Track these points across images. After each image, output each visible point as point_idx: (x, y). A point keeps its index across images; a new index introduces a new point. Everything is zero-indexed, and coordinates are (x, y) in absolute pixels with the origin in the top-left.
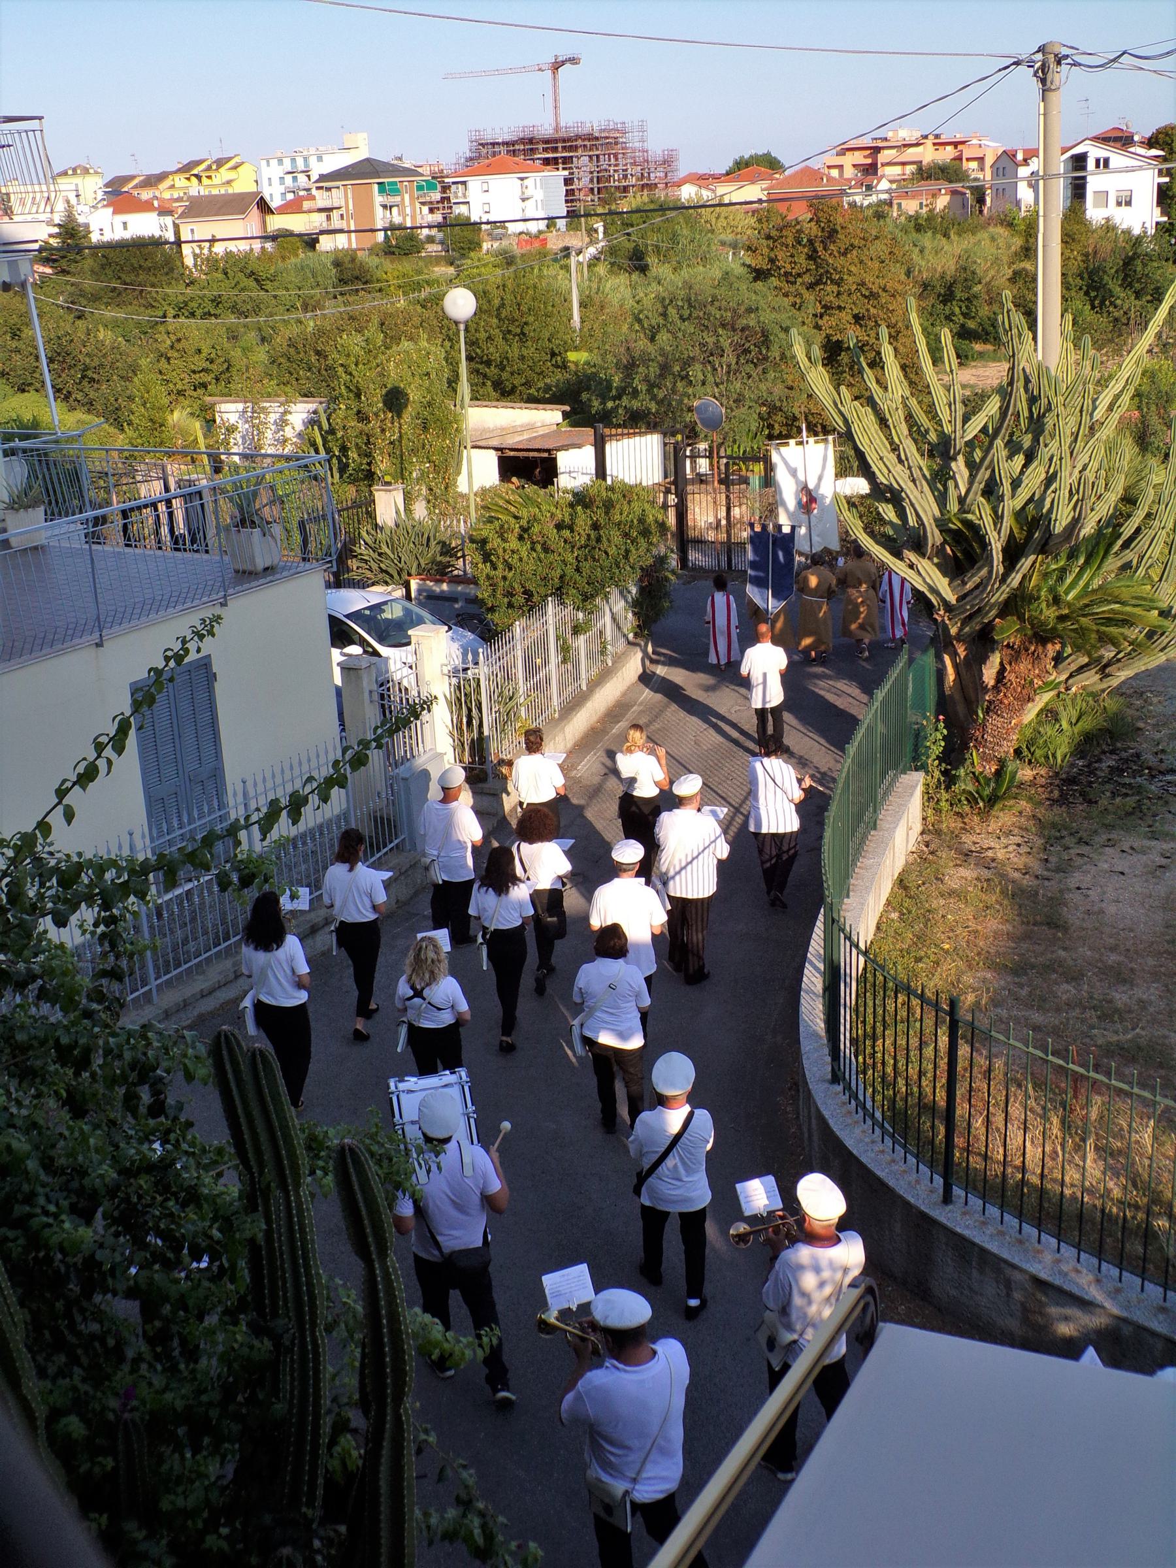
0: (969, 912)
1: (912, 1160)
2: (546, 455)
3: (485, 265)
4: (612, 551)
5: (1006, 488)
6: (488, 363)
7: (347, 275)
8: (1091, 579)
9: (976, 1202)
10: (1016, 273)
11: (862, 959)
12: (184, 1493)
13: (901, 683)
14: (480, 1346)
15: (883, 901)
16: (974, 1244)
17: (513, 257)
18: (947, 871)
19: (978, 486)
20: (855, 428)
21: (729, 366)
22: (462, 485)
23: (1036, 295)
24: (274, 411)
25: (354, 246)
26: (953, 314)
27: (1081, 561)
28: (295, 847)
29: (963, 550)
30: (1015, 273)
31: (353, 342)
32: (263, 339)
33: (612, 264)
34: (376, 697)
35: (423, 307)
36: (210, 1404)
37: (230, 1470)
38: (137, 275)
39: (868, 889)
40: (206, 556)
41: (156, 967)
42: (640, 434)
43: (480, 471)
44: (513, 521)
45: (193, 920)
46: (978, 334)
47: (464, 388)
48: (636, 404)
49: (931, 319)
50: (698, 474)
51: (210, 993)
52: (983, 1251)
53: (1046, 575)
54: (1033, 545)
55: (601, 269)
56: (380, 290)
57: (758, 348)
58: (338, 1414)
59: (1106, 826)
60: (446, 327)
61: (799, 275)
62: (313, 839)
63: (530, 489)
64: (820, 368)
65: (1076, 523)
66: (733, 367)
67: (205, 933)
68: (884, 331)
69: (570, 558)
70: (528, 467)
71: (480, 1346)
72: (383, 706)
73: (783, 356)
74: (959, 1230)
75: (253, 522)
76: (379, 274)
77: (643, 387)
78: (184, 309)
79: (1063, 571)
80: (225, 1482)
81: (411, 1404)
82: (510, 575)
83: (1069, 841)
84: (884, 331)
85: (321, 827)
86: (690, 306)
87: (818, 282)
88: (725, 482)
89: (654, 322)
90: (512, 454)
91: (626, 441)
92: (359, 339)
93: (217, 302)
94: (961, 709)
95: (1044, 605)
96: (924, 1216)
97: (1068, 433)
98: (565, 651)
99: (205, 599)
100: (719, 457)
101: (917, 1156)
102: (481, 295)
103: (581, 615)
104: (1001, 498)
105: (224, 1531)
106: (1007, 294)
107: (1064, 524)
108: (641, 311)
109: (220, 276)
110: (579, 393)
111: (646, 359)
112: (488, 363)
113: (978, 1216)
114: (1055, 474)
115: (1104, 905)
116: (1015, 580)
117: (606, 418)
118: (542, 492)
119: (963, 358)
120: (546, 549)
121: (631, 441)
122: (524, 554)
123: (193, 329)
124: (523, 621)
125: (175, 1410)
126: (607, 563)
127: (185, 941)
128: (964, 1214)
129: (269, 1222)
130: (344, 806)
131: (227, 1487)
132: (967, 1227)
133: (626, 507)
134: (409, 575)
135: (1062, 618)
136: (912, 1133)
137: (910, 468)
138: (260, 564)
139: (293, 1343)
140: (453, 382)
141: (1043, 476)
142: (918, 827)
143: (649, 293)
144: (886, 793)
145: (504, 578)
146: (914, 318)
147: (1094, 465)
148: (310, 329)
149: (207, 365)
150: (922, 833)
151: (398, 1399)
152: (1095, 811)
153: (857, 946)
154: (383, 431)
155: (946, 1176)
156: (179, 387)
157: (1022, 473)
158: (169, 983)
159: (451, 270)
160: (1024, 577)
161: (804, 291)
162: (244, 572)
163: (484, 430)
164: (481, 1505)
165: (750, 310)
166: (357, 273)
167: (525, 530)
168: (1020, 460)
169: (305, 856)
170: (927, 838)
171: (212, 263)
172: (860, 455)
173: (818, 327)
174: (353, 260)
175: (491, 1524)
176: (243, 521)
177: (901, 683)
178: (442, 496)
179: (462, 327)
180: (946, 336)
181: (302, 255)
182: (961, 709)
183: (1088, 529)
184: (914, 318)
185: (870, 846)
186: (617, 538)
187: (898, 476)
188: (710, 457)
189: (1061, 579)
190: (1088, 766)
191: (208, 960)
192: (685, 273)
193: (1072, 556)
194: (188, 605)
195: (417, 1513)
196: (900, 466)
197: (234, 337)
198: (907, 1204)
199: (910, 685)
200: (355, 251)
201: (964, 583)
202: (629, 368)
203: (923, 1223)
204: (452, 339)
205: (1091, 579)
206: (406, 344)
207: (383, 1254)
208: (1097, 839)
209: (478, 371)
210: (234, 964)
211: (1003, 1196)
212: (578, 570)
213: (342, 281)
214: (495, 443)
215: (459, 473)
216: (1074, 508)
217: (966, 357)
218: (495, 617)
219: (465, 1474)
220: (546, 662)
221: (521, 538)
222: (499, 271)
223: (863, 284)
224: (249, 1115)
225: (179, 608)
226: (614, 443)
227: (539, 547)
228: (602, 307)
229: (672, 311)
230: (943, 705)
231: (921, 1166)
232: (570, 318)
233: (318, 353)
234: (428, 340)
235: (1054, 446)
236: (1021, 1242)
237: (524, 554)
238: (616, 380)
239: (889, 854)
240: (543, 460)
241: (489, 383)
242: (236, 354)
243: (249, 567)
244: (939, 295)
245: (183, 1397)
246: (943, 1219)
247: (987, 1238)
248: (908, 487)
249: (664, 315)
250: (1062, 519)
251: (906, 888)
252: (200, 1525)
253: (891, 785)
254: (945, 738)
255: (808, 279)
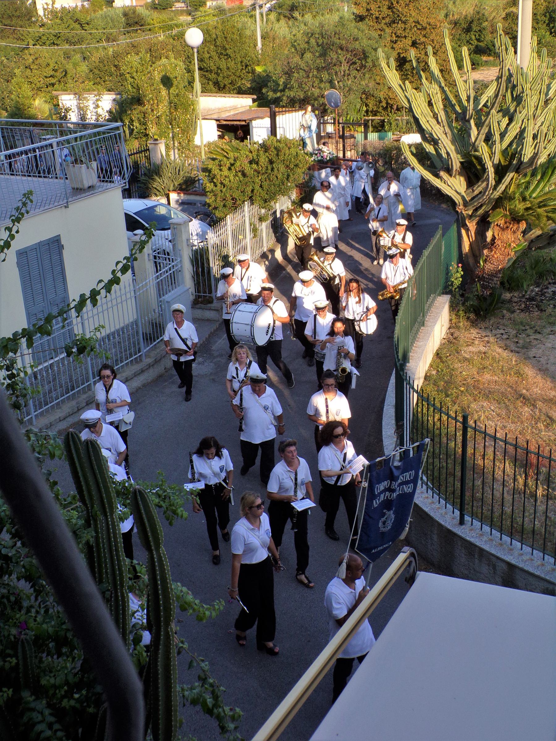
0: (474, 371)
1: (443, 502)
2: (243, 123)
3: (208, 15)
4: (280, 176)
5: (497, 137)
6: (211, 71)
7: (131, 21)
8: (544, 187)
9: (477, 524)
10: (508, 15)
11: (415, 395)
12: (54, 676)
13: (438, 247)
14: (214, 610)
15: (428, 365)
16: (476, 546)
17: (224, 10)
18: (462, 348)
19: (482, 137)
20: (414, 105)
21: (344, 71)
22: (197, 141)
23: (517, 27)
24: (91, 98)
25: (134, 4)
26: (471, 39)
27: (539, 177)
28: (109, 340)
29: (472, 171)
30: (507, 15)
31: (133, 59)
32: (84, 58)
33: (280, 14)
34: (152, 257)
35: (174, 39)
36: (67, 630)
37: (79, 664)
38: (12, 21)
39: (419, 359)
40: (56, 180)
41: (35, 406)
42: (295, 111)
43: (207, 133)
44: (225, 159)
45: (54, 380)
46: (483, 51)
47: (197, 85)
48: (292, 94)
49: (458, 43)
50: (327, 133)
51: (64, 419)
52: (481, 550)
53: (518, 186)
54: (512, 167)
55: (273, 16)
56: (150, 30)
57: (362, 60)
58: (136, 634)
59: (550, 323)
60: (186, 52)
61: (383, 18)
62: (119, 335)
63: (235, 142)
64: (395, 71)
65: (535, 156)
66: (347, 72)
67: (61, 387)
68: (430, 50)
69: (257, 180)
70: (235, 130)
71: (214, 610)
72: (155, 262)
73: (374, 66)
74: (468, 539)
75: (82, 161)
76: (149, 20)
77: (296, 85)
78: (38, 40)
79: (528, 183)
80: (76, 671)
81: (174, 626)
82: (224, 190)
83: (530, 332)
84: (430, 50)
85: (123, 329)
86: (322, 37)
87: (394, 22)
88: (343, 137)
89: (302, 46)
90: (225, 123)
91: (287, 114)
92: (137, 58)
93: (58, 36)
94: (471, 261)
95: (517, 202)
96: (449, 531)
97: (533, 105)
98: (255, 230)
99: (56, 204)
100: (339, 123)
101: (445, 500)
102: (206, 32)
103: (263, 211)
104: (494, 143)
105: (76, 696)
106: (500, 25)
107: (529, 157)
108: (295, 41)
109: (58, 21)
110: (261, 89)
111: (298, 68)
112: (211, 71)
113: (478, 531)
114: (525, 128)
115: (549, 366)
116: (502, 187)
117: (276, 102)
118: (241, 144)
119: (475, 65)
120: (244, 175)
121: (290, 114)
122: (232, 178)
123: (45, 52)
124: (231, 215)
125: (48, 633)
126: (277, 183)
127: (50, 391)
128: (471, 530)
129: (97, 532)
130: (135, 317)
131: (77, 673)
132: (473, 537)
133: (287, 152)
134: (169, 191)
135: (527, 209)
136: (443, 488)
137: (444, 127)
138: (86, 185)
139: (111, 597)
140: (191, 83)
141: (518, 130)
142: (447, 325)
143: (299, 31)
144: (430, 307)
145: (221, 191)
146: (447, 41)
147: (547, 124)
148: (110, 53)
149: (52, 73)
150: (449, 328)
151: (167, 624)
152: (544, 315)
153: (413, 388)
154: (152, 110)
155: (461, 510)
156: (38, 85)
157: (506, 128)
158: (42, 414)
159: (189, 18)
160: (506, 187)
161: (385, 27)
162: (77, 189)
163: (209, 110)
164: (211, 681)
165: (356, 39)
166: (136, 20)
167: (232, 165)
168: (506, 121)
169: (114, 344)
170: (452, 330)
171: (54, 13)
172: (416, 120)
173: (393, 48)
174: (134, 12)
175: (216, 690)
176: (76, 160)
177: (438, 247)
178: (186, 146)
179: (195, 50)
180: (465, 51)
181: (105, 10)
182: (471, 261)
183: (542, 159)
184: (447, 41)
185: (421, 335)
186: (282, 168)
187: (438, 131)
188: (334, 123)
189: (527, 188)
190: (541, 291)
191: (63, 401)
192: (320, 18)
193: (533, 175)
194: (46, 208)
195: (178, 689)
196: (438, 126)
197: (68, 57)
198: (440, 525)
199: (443, 247)
200: (135, 7)
201: (473, 191)
202: (289, 74)
203: (448, 536)
204: (189, 59)
205: (544, 187)
206: (164, 61)
207: (158, 547)
208: (545, 330)
209: (205, 76)
210: (77, 403)
211: (492, 521)
212: (261, 186)
213: (129, 25)
214: (215, 117)
215: (195, 134)
216: (535, 148)
217: (478, 64)
218: (218, 214)
219: (203, 665)
220: (245, 237)
221: (230, 169)
222: (216, 18)
223: (418, 22)
224: (82, 470)
225: (42, 209)
226: (281, 116)
227: (240, 174)
228: (274, 39)
229: (313, 41)
230: (461, 259)
231: (448, 505)
232: (255, 45)
233: (116, 66)
234: (175, 59)
235: (524, 112)
236: (501, 545)
237: (232, 178)
238: (281, 82)
239: (431, 339)
240: (242, 126)
241: (211, 83)
242: (69, 67)
243: (80, 186)
244: (464, 29)
245: (52, 627)
246: (459, 533)
247: (483, 543)
248: (442, 137)
249: (308, 43)
250: (528, 153)
251: (440, 358)
252: (63, 693)
253: (432, 302)
254: (462, 276)
255: (387, 20)
